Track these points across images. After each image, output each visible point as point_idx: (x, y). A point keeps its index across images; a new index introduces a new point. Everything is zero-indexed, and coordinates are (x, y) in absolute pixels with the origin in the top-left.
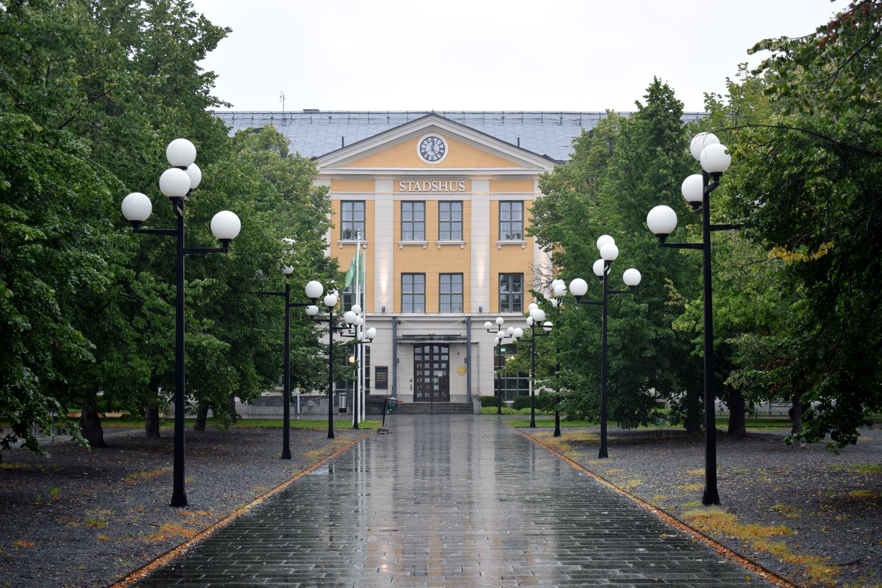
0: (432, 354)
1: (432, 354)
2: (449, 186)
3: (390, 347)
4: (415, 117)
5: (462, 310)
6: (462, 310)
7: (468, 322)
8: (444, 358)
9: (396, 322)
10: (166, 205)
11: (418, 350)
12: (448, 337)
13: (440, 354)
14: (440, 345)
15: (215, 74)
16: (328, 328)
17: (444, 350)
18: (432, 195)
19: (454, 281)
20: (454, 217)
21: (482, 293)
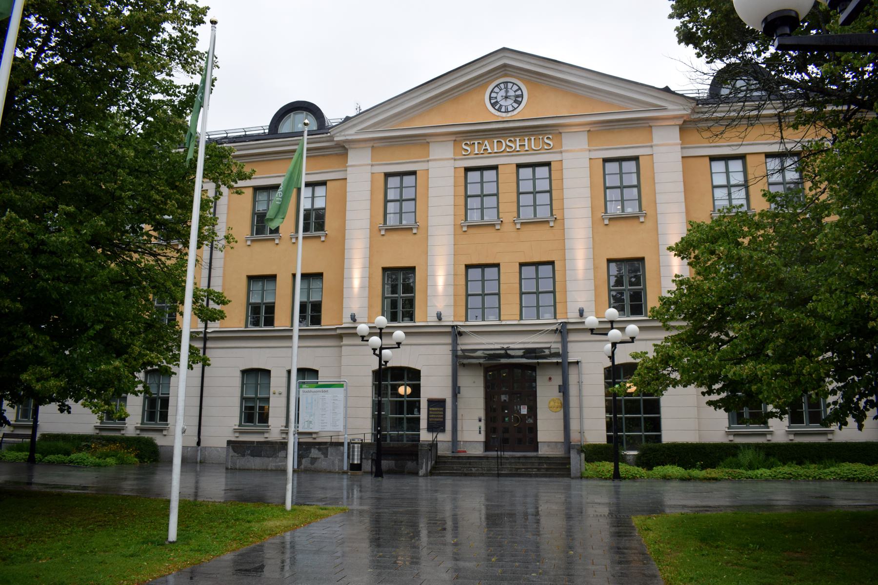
7: (563, 331)
9: (456, 333)
18: (506, 156)
19: (542, 270)
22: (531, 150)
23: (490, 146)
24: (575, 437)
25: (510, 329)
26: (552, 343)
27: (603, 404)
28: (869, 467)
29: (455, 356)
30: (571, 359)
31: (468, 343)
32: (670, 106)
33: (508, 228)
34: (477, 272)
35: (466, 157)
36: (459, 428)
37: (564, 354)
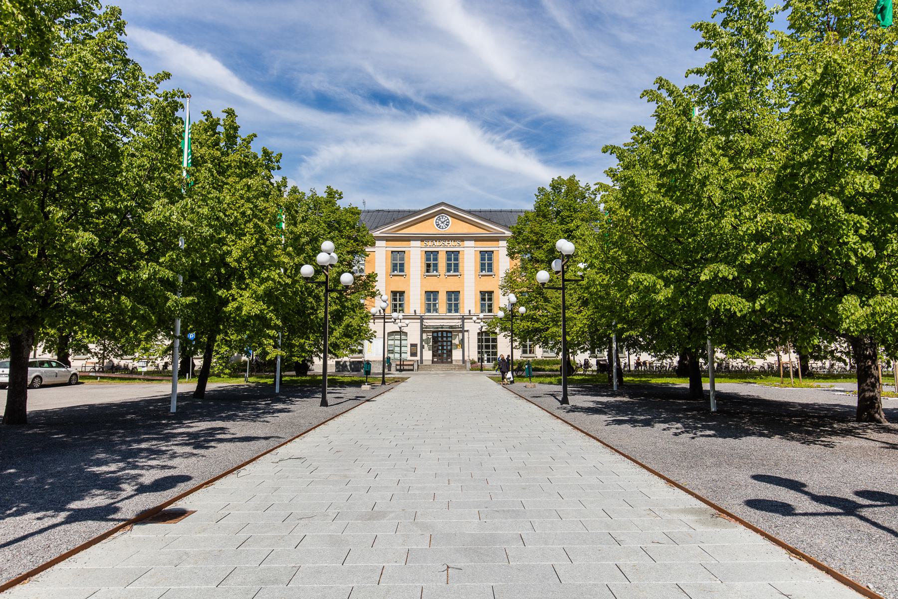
0: (442, 337)
1: (442, 337)
2: (452, 243)
3: (419, 333)
4: (406, 214)
5: (456, 311)
6: (456, 311)
7: (463, 319)
8: (449, 339)
9: (422, 319)
10: (320, 269)
11: (435, 335)
12: (451, 327)
13: (447, 337)
14: (447, 332)
15: (699, 37)
16: (856, 389)
17: (449, 335)
18: (442, 248)
19: (454, 296)
20: (454, 262)
21: (470, 303)
22: (452, 246)
23: (437, 243)
24: (466, 358)
25: (442, 319)
26: (458, 323)
27: (376, 264)
28: (737, 440)
29: (422, 328)
30: (466, 329)
31: (427, 323)
32: (506, 232)
33: (442, 277)
34: (431, 296)
35: (426, 247)
36: (115, 535)
37: (463, 327)
